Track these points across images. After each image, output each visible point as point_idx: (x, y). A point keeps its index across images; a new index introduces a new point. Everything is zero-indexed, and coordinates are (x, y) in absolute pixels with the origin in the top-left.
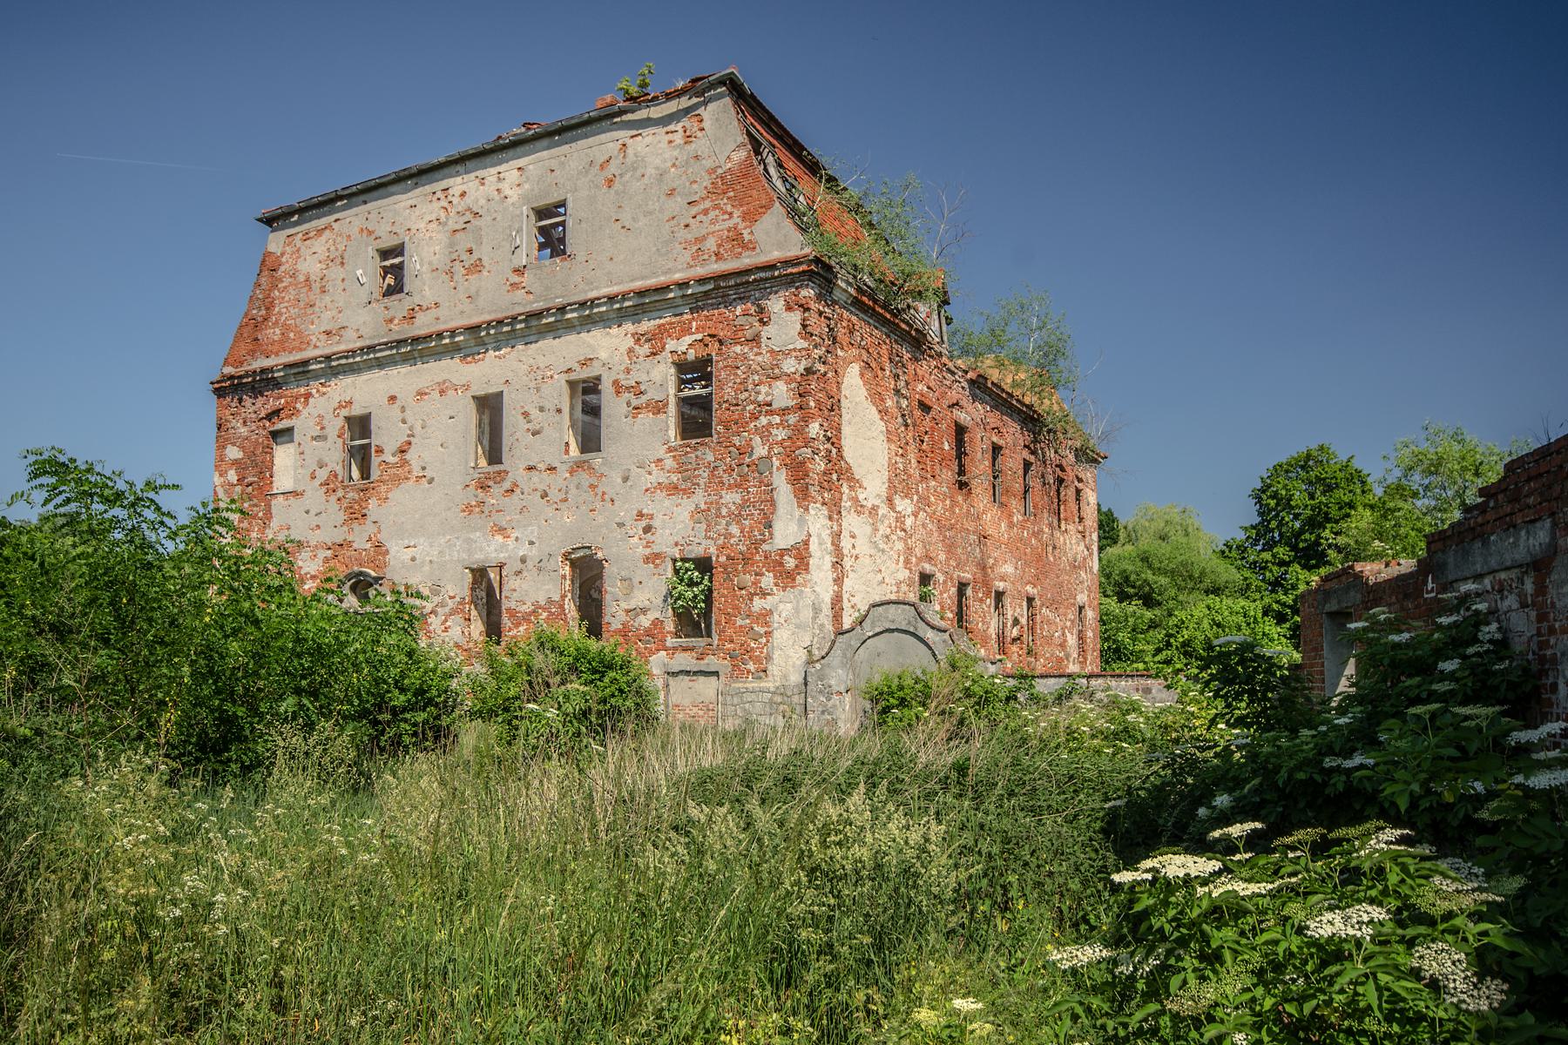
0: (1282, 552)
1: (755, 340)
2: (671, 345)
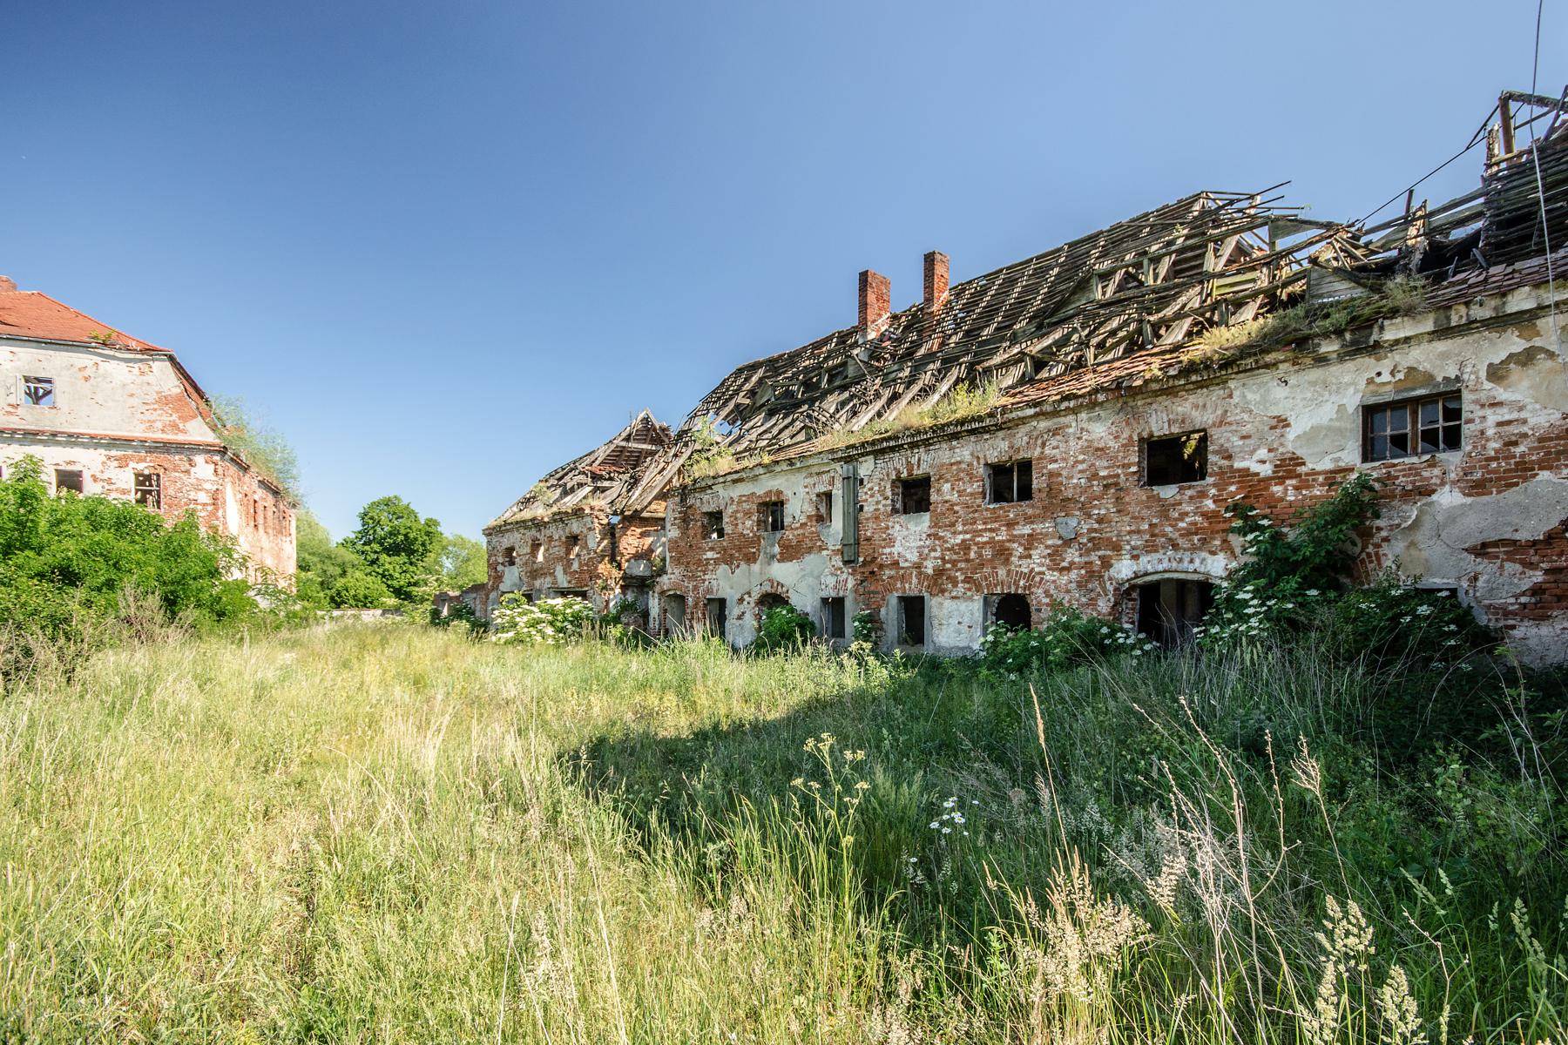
0: (376, 547)
1: (187, 472)
2: (132, 465)
